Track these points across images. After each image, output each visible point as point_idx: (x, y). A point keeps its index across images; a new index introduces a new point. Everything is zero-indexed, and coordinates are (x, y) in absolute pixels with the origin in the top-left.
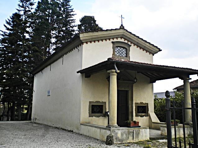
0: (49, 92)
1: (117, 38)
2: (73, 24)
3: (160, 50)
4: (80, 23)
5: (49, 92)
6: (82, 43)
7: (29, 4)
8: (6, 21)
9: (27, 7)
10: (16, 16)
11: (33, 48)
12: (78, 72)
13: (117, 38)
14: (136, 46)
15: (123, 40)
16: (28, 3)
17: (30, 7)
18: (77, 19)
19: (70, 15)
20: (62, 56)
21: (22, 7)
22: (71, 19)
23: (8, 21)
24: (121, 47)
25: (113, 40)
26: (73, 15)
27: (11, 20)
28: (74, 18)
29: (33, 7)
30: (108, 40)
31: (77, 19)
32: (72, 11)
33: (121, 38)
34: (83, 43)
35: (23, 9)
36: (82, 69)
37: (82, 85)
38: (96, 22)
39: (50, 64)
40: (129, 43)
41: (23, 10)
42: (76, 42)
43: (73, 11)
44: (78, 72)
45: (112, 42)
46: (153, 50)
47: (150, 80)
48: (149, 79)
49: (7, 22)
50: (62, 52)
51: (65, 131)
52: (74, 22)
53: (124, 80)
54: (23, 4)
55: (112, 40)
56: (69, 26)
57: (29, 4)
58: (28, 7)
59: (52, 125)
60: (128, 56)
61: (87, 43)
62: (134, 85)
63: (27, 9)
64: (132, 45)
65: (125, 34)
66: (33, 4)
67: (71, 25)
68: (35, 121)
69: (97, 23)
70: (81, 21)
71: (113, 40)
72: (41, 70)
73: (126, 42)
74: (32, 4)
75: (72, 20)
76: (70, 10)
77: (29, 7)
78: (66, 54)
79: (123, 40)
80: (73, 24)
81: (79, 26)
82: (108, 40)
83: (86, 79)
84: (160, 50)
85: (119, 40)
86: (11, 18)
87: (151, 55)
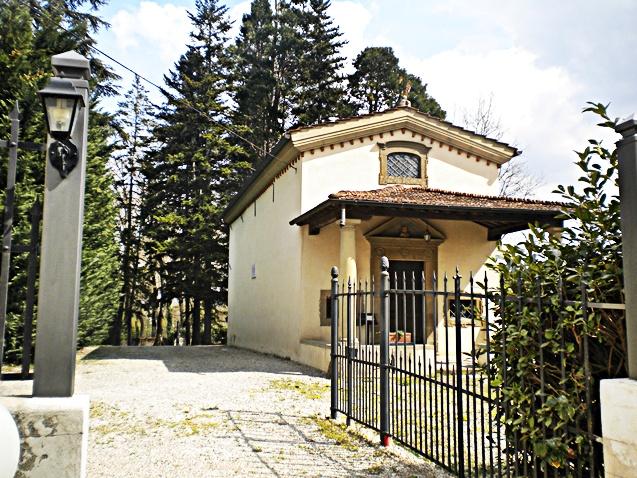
0: (254, 269)
1: (392, 133)
2: (339, 73)
3: (516, 153)
4: (352, 71)
5: (254, 269)
6: (300, 154)
7: (218, 28)
8: (167, 79)
9: (212, 37)
10: (190, 64)
11: (230, 149)
12: (292, 223)
13: (392, 133)
14: (445, 148)
15: (407, 137)
16: (215, 25)
17: (221, 35)
18: (347, 55)
19: (330, 46)
20: (271, 183)
21: (200, 38)
22: (335, 56)
23: (170, 76)
24: (402, 154)
25: (381, 137)
26: (338, 45)
27: (177, 72)
28: (342, 52)
29: (228, 34)
30: (366, 140)
31: (347, 55)
32: (336, 34)
33: (403, 130)
34: (302, 154)
35: (203, 43)
36: (303, 213)
37: (302, 259)
38: (399, 64)
39: (254, 200)
40: (427, 142)
41: (204, 47)
42: (287, 155)
43: (339, 32)
44: (292, 223)
45: (381, 146)
46: (496, 154)
47: (372, 245)
48: (485, 230)
49: (168, 80)
50: (269, 171)
51: (236, 351)
52: (341, 65)
53: (410, 237)
54: (202, 32)
55: (377, 139)
56: (330, 79)
57: (218, 28)
58: (215, 35)
59: (260, 350)
60: (423, 175)
61: (312, 151)
62: (440, 247)
63: (215, 42)
64: (436, 145)
65: (411, 121)
66: (229, 27)
67: (335, 75)
68: (233, 343)
69: (401, 65)
70: (356, 65)
71: (381, 137)
72: (241, 214)
73: (417, 139)
74: (225, 27)
75: (338, 60)
76: (329, 31)
77: (218, 35)
78: (278, 175)
79: (407, 137)
80: (339, 73)
81: (354, 80)
82: (366, 140)
83: (313, 237)
84: (516, 153)
85: (398, 136)
86: (178, 68)
87: (493, 167)
